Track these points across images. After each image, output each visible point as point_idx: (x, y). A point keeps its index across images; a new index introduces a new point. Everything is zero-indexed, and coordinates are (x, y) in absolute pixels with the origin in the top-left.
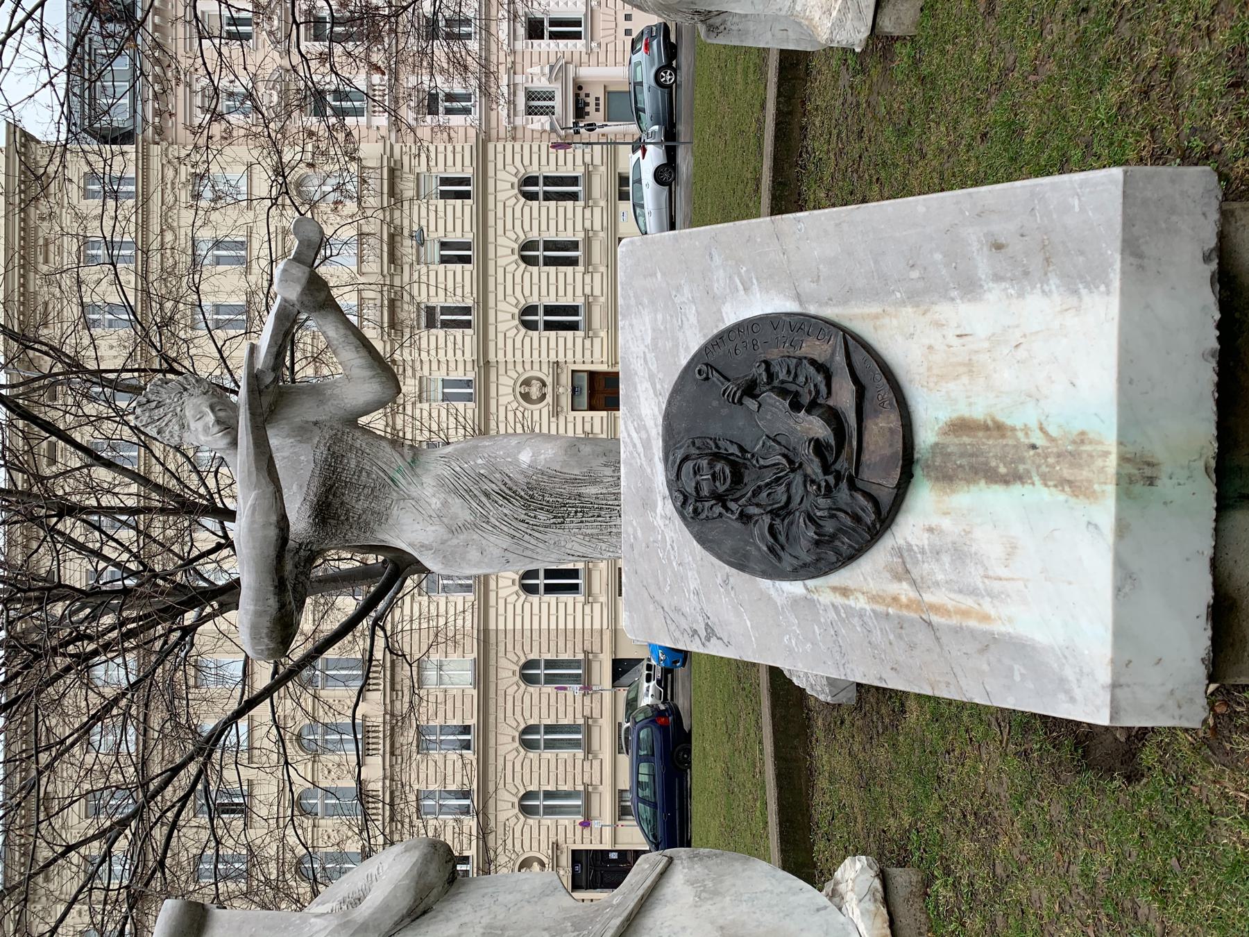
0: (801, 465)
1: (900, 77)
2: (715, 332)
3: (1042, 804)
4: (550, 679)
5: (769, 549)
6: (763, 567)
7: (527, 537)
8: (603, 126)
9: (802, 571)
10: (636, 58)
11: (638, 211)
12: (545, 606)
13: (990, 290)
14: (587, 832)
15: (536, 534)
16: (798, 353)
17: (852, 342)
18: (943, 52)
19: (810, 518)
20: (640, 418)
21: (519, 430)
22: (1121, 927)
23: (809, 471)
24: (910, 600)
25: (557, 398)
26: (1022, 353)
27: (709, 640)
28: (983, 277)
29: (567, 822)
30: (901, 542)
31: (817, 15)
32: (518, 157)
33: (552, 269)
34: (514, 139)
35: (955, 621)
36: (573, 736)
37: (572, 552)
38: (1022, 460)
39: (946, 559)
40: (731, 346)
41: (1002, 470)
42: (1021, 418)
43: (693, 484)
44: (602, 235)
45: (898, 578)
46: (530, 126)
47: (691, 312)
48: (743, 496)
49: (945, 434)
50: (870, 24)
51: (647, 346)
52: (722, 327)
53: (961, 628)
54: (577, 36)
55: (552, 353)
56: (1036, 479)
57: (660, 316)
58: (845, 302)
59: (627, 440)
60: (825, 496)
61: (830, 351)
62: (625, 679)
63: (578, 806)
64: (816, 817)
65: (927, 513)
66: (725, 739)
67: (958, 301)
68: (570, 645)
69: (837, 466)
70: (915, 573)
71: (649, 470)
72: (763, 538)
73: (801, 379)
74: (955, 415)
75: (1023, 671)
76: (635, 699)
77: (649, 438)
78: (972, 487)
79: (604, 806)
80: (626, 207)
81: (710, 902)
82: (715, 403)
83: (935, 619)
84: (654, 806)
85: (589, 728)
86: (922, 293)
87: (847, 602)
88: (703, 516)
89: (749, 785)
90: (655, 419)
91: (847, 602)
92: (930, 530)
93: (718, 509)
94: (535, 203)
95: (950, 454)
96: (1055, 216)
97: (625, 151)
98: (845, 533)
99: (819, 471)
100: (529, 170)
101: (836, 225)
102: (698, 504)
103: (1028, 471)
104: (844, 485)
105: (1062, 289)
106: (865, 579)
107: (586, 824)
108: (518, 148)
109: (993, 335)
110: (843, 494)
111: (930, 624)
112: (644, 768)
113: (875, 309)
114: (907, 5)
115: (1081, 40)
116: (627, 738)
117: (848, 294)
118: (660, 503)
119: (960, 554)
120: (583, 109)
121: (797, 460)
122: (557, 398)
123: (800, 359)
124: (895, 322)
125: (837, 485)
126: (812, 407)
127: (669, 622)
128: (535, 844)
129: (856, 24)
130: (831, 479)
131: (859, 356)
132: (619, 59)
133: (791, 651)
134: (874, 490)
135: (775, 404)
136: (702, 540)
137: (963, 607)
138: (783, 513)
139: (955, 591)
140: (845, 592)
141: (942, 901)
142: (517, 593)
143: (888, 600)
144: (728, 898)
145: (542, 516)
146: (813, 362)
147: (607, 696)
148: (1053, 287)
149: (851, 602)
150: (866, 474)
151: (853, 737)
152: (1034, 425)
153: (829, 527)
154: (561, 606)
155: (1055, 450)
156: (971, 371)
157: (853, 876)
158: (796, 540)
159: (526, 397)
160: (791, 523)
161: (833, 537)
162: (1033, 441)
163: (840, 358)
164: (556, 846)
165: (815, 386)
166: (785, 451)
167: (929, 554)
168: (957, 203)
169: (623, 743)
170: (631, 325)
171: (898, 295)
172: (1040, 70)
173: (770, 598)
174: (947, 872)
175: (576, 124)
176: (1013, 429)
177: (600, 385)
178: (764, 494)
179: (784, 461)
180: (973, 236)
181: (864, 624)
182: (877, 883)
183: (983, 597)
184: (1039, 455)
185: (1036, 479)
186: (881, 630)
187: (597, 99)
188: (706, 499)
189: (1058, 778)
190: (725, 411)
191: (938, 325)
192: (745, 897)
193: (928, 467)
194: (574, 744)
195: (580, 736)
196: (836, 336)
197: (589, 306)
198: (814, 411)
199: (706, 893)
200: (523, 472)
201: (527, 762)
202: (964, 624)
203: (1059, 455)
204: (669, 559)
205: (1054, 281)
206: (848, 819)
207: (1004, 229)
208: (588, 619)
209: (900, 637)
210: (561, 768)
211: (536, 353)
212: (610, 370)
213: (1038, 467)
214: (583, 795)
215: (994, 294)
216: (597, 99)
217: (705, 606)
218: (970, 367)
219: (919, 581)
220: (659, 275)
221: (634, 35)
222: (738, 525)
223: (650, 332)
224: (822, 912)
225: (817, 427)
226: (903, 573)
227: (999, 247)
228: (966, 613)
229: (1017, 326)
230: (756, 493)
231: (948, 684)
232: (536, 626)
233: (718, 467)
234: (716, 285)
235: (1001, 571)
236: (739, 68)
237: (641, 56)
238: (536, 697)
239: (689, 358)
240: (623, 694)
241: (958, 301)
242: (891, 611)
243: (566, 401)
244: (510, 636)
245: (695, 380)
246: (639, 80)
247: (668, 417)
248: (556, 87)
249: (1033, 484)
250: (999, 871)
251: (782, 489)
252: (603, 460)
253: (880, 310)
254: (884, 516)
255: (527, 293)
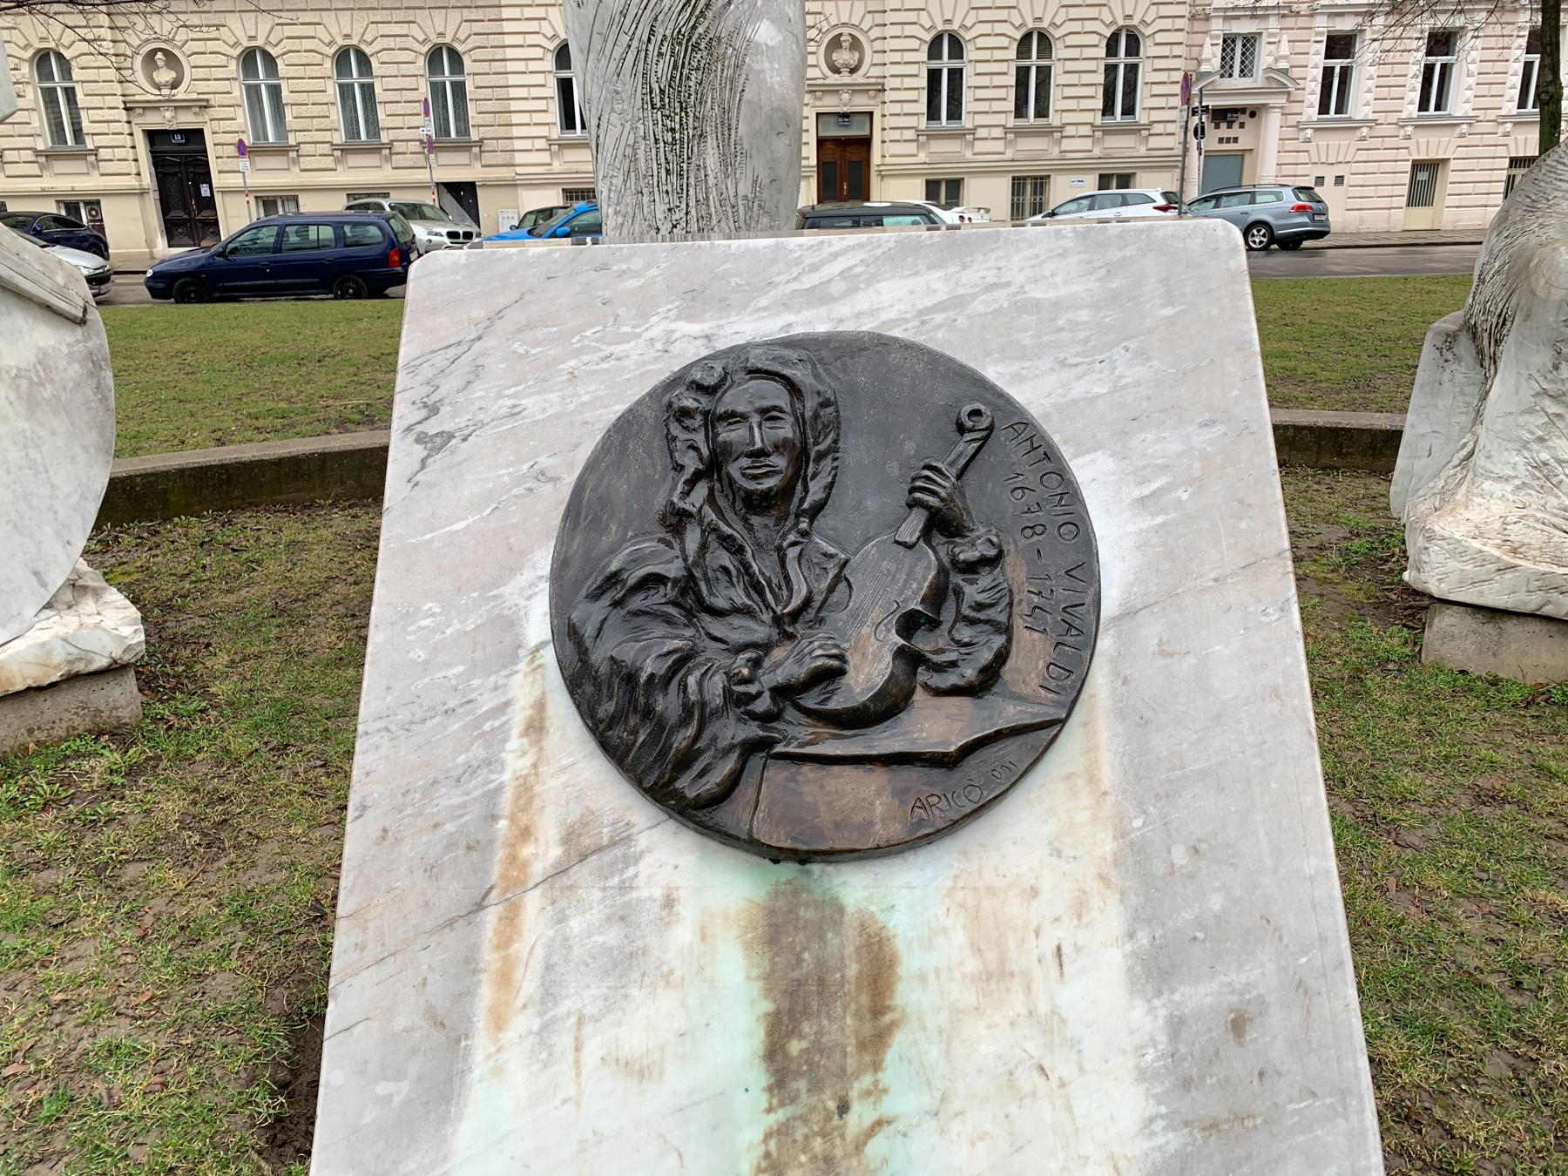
0: (791, 637)
1: (1353, 634)
2: (1056, 439)
3: (234, 955)
4: (438, 90)
5: (615, 574)
6: (576, 562)
7: (625, 39)
8: (1199, 148)
9: (571, 639)
10: (1288, 194)
11: (1085, 202)
12: (539, 79)
13: (1151, 1010)
14: (232, 150)
15: (631, 57)
16: (1018, 623)
17: (1042, 732)
18: (1404, 713)
19: (683, 660)
20: (872, 279)
21: (810, 20)
22: (21, 1131)
23: (778, 654)
24: (525, 865)
25: (833, 90)
26: (1028, 1079)
27: (418, 440)
28: (1177, 997)
29: (241, 120)
30: (642, 842)
31: (1474, 515)
32: (1167, 24)
33: (1100, 78)
34: (1193, 18)
35: (489, 957)
36: (362, 131)
37: (604, 125)
38: (816, 1086)
39: (613, 936)
40: (1031, 479)
41: (795, 1047)
42: (901, 1085)
43: (740, 409)
44: (1055, 152)
45: (569, 838)
46: (1208, 41)
47: (1093, 385)
48: (720, 513)
49: (863, 927)
50: (1452, 597)
51: (1021, 290)
52: (1066, 452)
53: (476, 971)
54: (1324, 109)
55: (896, 83)
56: (780, 1115)
57: (1084, 315)
58: (1120, 713)
59: (826, 251)
60: (728, 692)
61: (1026, 691)
62: (450, 201)
63: (266, 138)
64: (241, 518)
65: (699, 893)
66: (373, 351)
67: (1128, 947)
68: (489, 119)
69: (790, 714)
70: (581, 873)
71: (764, 302)
72: (636, 560)
73: (965, 633)
74: (900, 945)
75: (397, 1100)
76: (423, 217)
77: (830, 299)
78: (759, 984)
79: (272, 176)
80: (1090, 185)
81: (13, 397)
82: (910, 447)
83: (491, 916)
84: (277, 249)
85: (377, 150)
86: (1144, 873)
87: (515, 732)
88: (675, 429)
89: (309, 389)
90: (871, 313)
91: (515, 732)
92: (669, 902)
93: (691, 463)
94: (1102, 52)
95: (822, 938)
96: (1301, 1139)
97: (1169, 181)
98: (654, 738)
99: (780, 677)
100: (1149, 42)
101: (1275, 689)
102: (699, 420)
103: (794, 1100)
104: (753, 730)
105: (1157, 1157)
106: (563, 770)
107: (242, 148)
108: (1180, 23)
109: (1064, 1021)
110: (733, 731)
111: (480, 906)
112: (327, 233)
113: (1109, 774)
114: (1472, 649)
115: (1474, 981)
116: (367, 206)
117: (1137, 719)
118: (696, 328)
119: (624, 965)
120: (1224, 119)
121: (799, 628)
122: (833, 90)
123: (1007, 630)
124: (1083, 817)
125: (754, 716)
126: (910, 659)
127: (451, 353)
128: (201, 73)
129: (1454, 577)
130: (763, 704)
131: (1010, 750)
132: (1287, 170)
133: (409, 616)
134: (745, 792)
135: (911, 582)
136: (625, 426)
137: (518, 974)
138: (690, 601)
139: (548, 956)
140: (536, 727)
141: (86, 765)
142: (555, 36)
143: (524, 819)
144: (26, 425)
145: (663, 68)
146: (1002, 657)
147: (422, 176)
148: (1161, 1140)
149: (515, 742)
150: (777, 775)
151: (356, 583)
152: (888, 1107)
153: (667, 704)
154: (541, 105)
155: (839, 1152)
156: (990, 976)
157: (108, 623)
158: (636, 634)
159: (835, 43)
160: (669, 620)
161: (648, 713)
162: (856, 1107)
163: (1010, 713)
164: (206, 106)
165: (953, 664)
166: (818, 599)
167: (620, 900)
168: (1322, 939)
169: (363, 201)
170: (1064, 254)
171: (1138, 823)
172: (1404, 896)
173: (515, 570)
174: (133, 772)
175: (1206, 109)
176: (877, 1066)
177: (852, 155)
178: (726, 559)
179: (796, 602)
180: (1259, 974)
181: (472, 770)
182: (101, 662)
183: (540, 1014)
184: (828, 1119)
185: (780, 1115)
186: (464, 805)
187: (1236, 140)
188: (711, 437)
189: (277, 984)
190: (893, 469)
191: (1080, 909)
192: (33, 454)
193: (795, 893)
194: (352, 131)
195: (453, 135)
196: (1057, 704)
197: (960, 135)
198: (901, 664)
199: (30, 386)
200: (738, 29)
201: (317, 58)
202: (483, 977)
203: (828, 1160)
204: (579, 352)
205: (1173, 1141)
206: (230, 580)
207: (1274, 1035)
208: (527, 144)
209: (450, 845)
210: (316, 110)
211: (896, 57)
212: (873, 168)
213: (804, 1119)
214: (282, 143)
215: (1144, 1020)
216: (1236, 140)
217: (488, 430)
218: (996, 976)
219: (566, 881)
220: (1168, 311)
221: (1317, 190)
222: (659, 503)
223: (1052, 295)
224: (34, 580)
225: (869, 671)
226: (581, 847)
227: (1238, 1026)
228: (505, 979)
229: (1081, 1069)
230: (727, 542)
231: (361, 947)
232: (511, 66)
233: (779, 462)
234: (1150, 436)
235: (593, 1050)
236: (1285, 345)
237: (1290, 200)
238: (410, 69)
239: (1001, 384)
240: (428, 198)
241: (1128, 947)
242: (503, 824)
243: (831, 104)
244: (493, 27)
245: (958, 402)
246: (1259, 199)
247: (874, 347)
248: (1257, 80)
249: (770, 1110)
250: (133, 870)
251: (740, 596)
252: (764, 178)
253: (1106, 785)
254: (699, 814)
255: (981, 42)
